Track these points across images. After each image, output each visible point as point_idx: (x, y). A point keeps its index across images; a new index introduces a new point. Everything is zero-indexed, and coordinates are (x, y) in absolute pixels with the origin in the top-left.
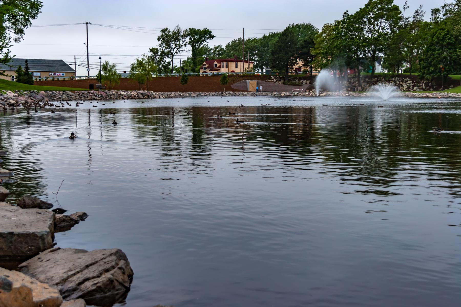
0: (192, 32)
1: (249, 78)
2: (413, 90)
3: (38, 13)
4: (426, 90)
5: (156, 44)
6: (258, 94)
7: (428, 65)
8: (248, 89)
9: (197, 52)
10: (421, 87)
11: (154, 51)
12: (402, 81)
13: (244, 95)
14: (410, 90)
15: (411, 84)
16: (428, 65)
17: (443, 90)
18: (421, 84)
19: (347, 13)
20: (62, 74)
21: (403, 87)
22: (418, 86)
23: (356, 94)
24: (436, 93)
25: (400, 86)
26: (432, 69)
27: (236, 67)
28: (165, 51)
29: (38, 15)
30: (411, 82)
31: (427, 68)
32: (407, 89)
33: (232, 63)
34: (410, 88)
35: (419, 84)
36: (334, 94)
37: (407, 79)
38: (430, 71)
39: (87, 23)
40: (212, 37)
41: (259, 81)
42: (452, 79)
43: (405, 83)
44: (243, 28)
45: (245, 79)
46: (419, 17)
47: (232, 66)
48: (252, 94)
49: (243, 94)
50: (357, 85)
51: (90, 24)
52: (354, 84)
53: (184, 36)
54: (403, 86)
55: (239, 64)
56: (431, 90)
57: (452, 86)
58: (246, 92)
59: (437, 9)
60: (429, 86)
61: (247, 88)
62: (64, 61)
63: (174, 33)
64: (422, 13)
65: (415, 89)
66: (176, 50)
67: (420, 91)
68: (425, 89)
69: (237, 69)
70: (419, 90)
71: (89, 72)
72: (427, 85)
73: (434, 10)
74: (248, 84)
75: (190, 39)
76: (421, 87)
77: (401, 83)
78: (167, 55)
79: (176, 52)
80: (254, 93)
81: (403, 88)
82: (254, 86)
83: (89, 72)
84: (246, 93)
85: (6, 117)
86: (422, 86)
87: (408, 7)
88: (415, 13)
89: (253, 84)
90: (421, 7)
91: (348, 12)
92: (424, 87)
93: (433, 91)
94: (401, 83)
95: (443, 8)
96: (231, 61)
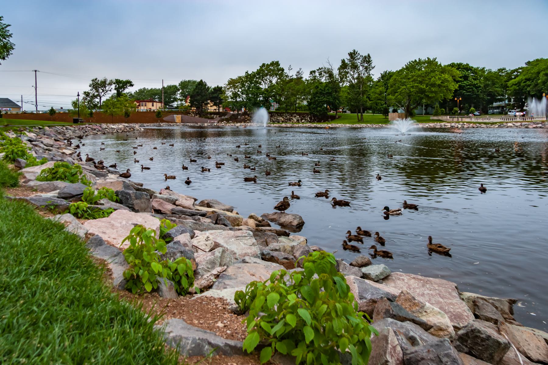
0: (118, 82)
3: (9, 54)
5: (88, 89)
9: (119, 94)
11: (87, 94)
17: (324, 121)
20: (8, 109)
27: (153, 105)
28: (168, 91)
29: (9, 56)
30: (298, 117)
39: (36, 71)
40: (132, 85)
41: (183, 115)
47: (149, 105)
51: (39, 71)
53: (110, 84)
61: (174, 120)
62: (10, 98)
63: (102, 82)
65: (303, 121)
66: (103, 93)
71: (37, 108)
72: (311, 118)
75: (116, 86)
78: (96, 97)
79: (103, 95)
83: (37, 108)
90: (300, 69)
92: (309, 120)
95: (318, 70)
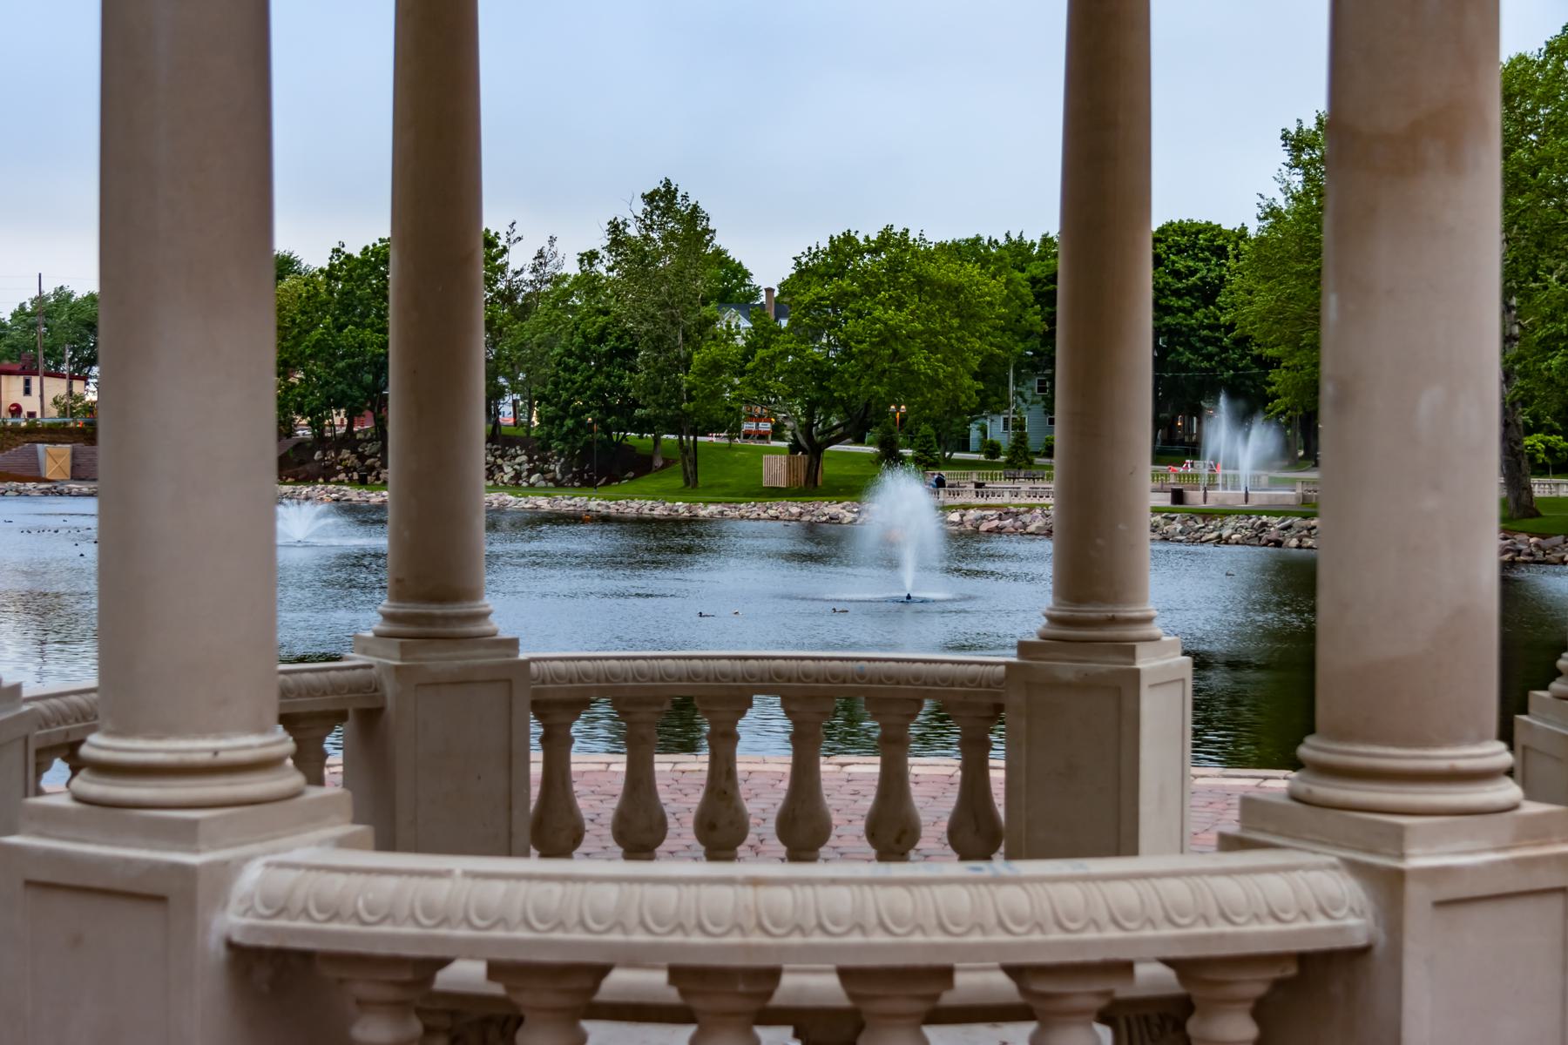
1: (48, 436)
2: (528, 482)
4: (562, 486)
6: (66, 491)
7: (561, 413)
8: (43, 471)
10: (549, 476)
12: (502, 457)
13: (19, 493)
14: (520, 482)
15: (526, 466)
16: (561, 413)
18: (552, 467)
19: (343, 249)
21: (502, 474)
22: (543, 472)
23: (359, 494)
24: (560, 497)
25: (496, 471)
26: (571, 425)
27: (27, 392)
31: (557, 422)
32: (512, 478)
33: (13, 378)
34: (521, 478)
35: (546, 466)
36: (297, 492)
37: (516, 450)
38: (565, 429)
41: (79, 446)
42: (637, 451)
43: (509, 463)
44: (40, 274)
45: (34, 439)
46: (548, 269)
48: (47, 489)
49: (17, 491)
50: (379, 463)
52: (369, 462)
54: (503, 470)
55: (35, 381)
56: (576, 484)
57: (631, 474)
58: (28, 484)
59: (591, 252)
60: (571, 472)
61: (39, 469)
64: (556, 259)
65: (533, 479)
67: (546, 487)
68: (561, 480)
69: (27, 398)
70: (543, 483)
73: (585, 254)
74: (41, 455)
76: (549, 476)
77: (499, 461)
80: (55, 488)
81: (502, 477)
82: (60, 461)
84: (30, 485)
85: (459, 658)
86: (554, 471)
87: (520, 239)
88: (536, 258)
89: (60, 456)
91: (343, 246)
92: (559, 476)
93: (579, 487)
94: (499, 461)
96: (9, 373)
